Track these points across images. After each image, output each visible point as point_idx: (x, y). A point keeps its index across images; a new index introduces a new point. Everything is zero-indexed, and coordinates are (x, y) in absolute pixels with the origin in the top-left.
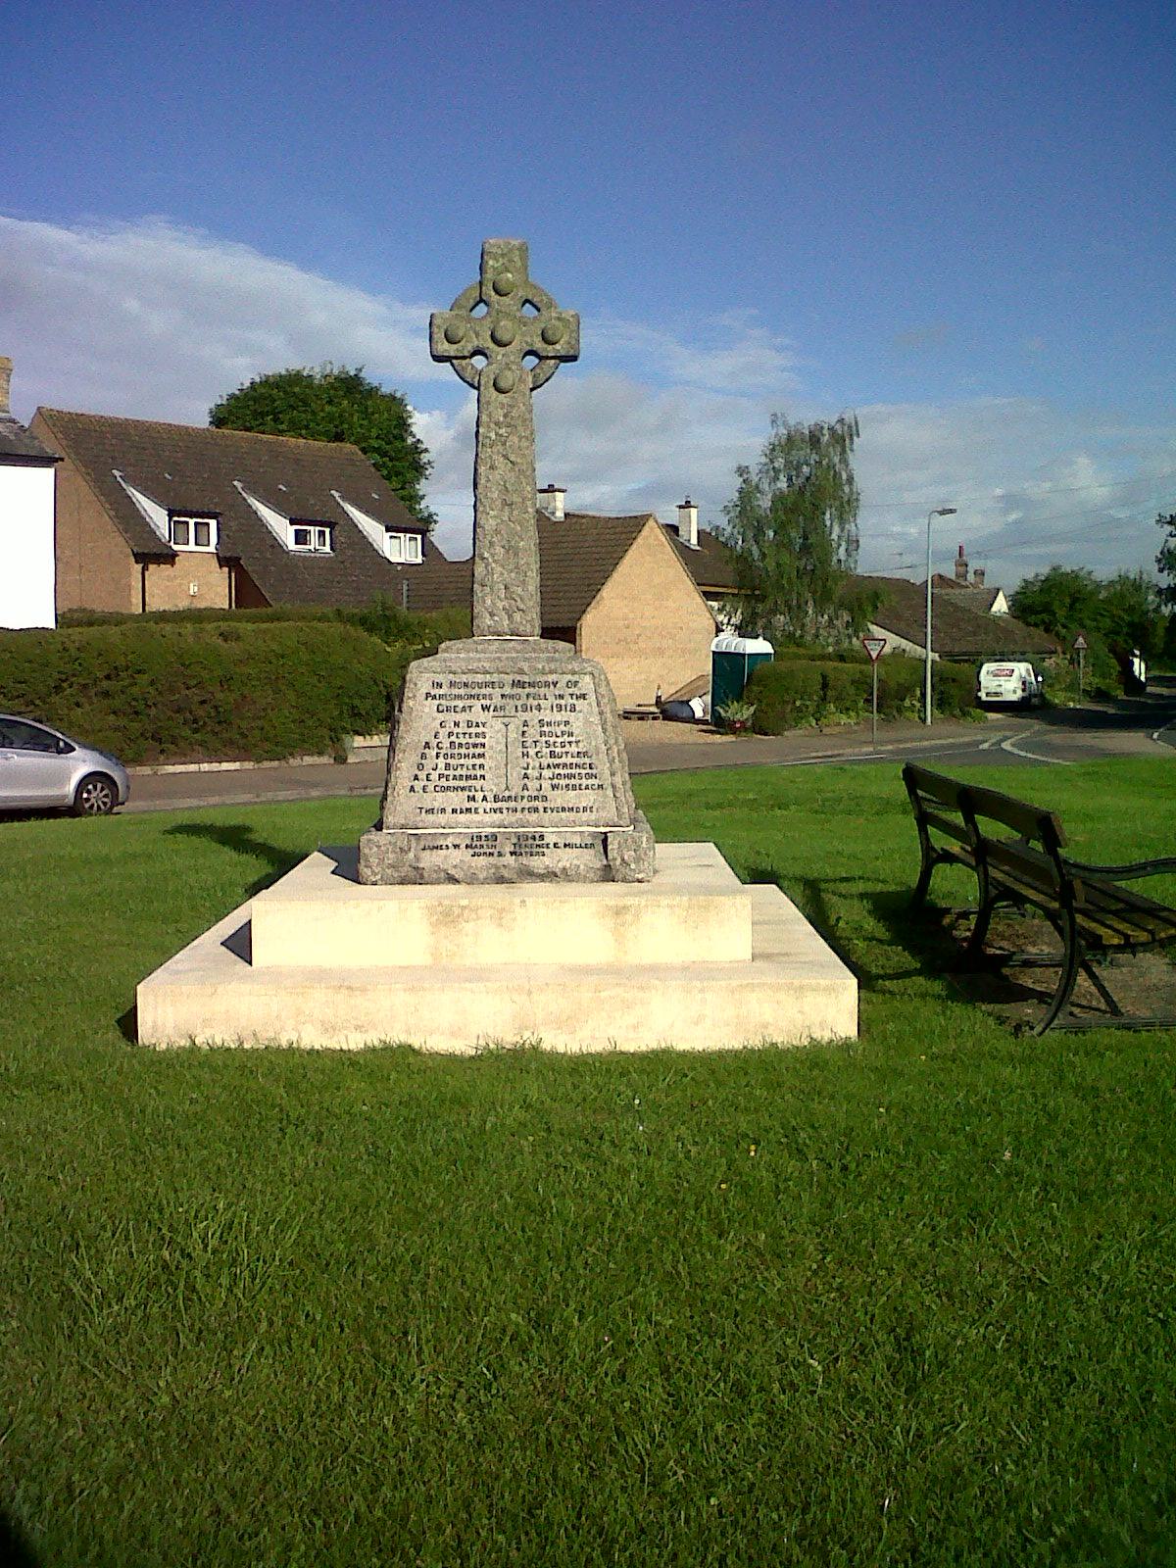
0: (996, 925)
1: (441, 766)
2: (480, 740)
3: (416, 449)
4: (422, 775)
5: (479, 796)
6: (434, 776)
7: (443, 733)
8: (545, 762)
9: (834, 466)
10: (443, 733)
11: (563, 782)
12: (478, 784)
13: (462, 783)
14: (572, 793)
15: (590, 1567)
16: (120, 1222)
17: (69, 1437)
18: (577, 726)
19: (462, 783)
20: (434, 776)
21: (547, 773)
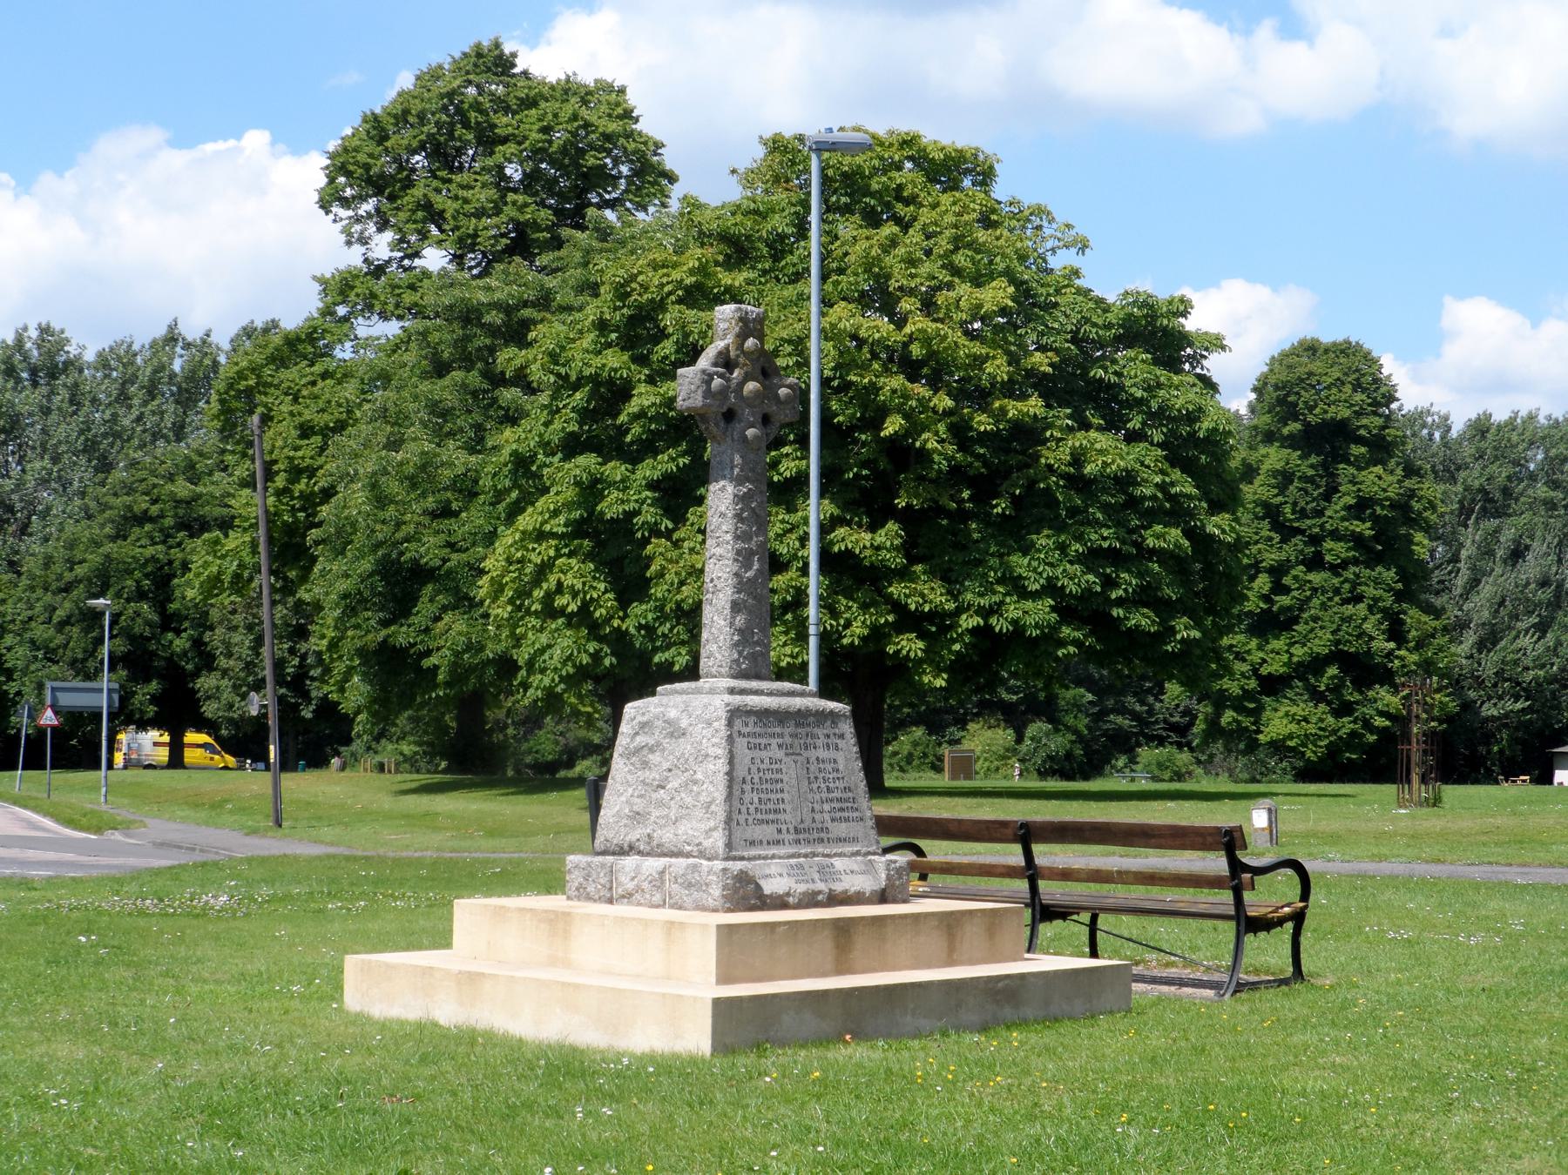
0: (1248, 896)
1: (756, 800)
2: (779, 776)
3: (146, 731)
4: (744, 810)
5: (784, 827)
6: (752, 810)
7: (754, 769)
8: (824, 795)
9: (588, 730)
10: (754, 769)
11: (838, 815)
12: (781, 817)
13: (771, 817)
14: (844, 825)
15: (1566, 861)
16: (1148, 617)
17: (1400, 971)
18: (840, 757)
19: (771, 817)
20: (752, 810)
21: (826, 807)
